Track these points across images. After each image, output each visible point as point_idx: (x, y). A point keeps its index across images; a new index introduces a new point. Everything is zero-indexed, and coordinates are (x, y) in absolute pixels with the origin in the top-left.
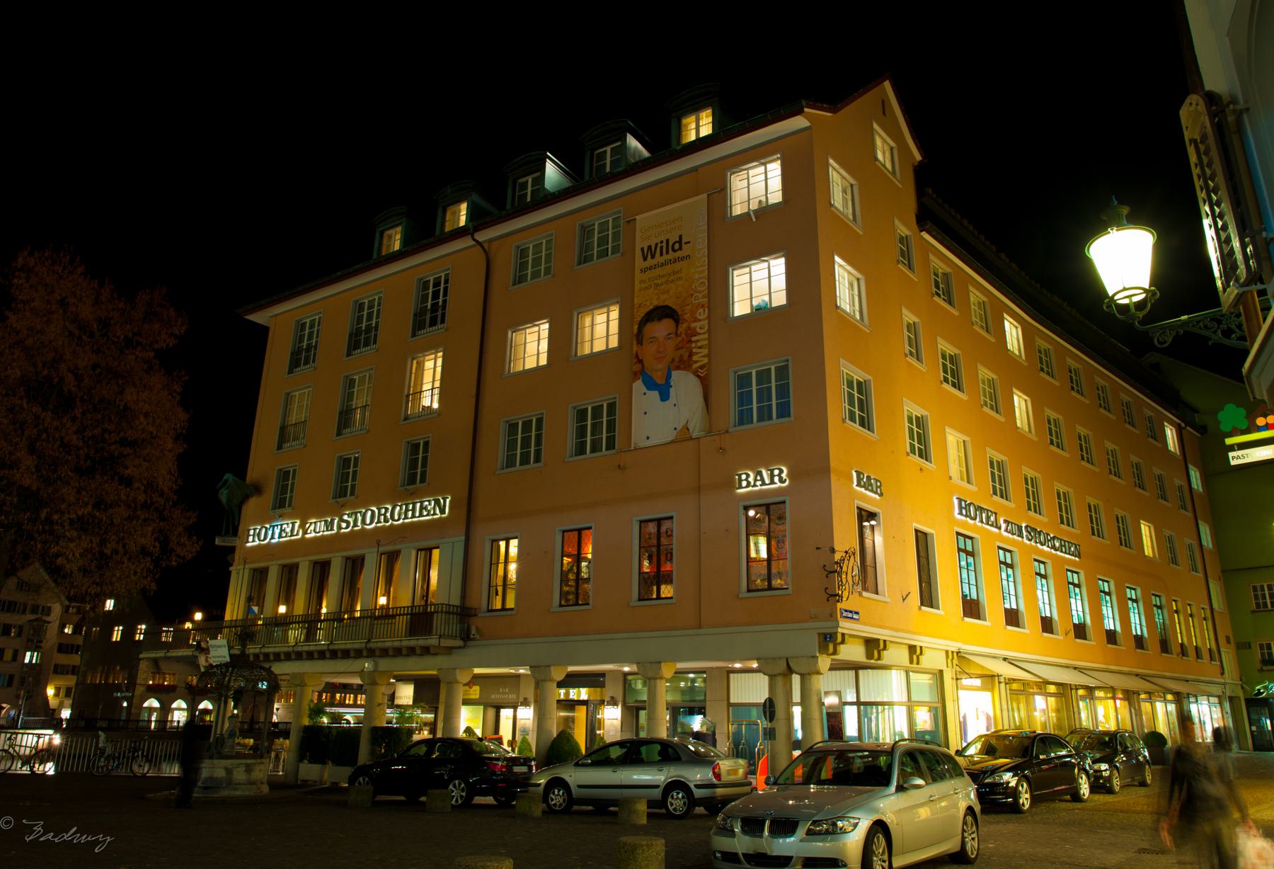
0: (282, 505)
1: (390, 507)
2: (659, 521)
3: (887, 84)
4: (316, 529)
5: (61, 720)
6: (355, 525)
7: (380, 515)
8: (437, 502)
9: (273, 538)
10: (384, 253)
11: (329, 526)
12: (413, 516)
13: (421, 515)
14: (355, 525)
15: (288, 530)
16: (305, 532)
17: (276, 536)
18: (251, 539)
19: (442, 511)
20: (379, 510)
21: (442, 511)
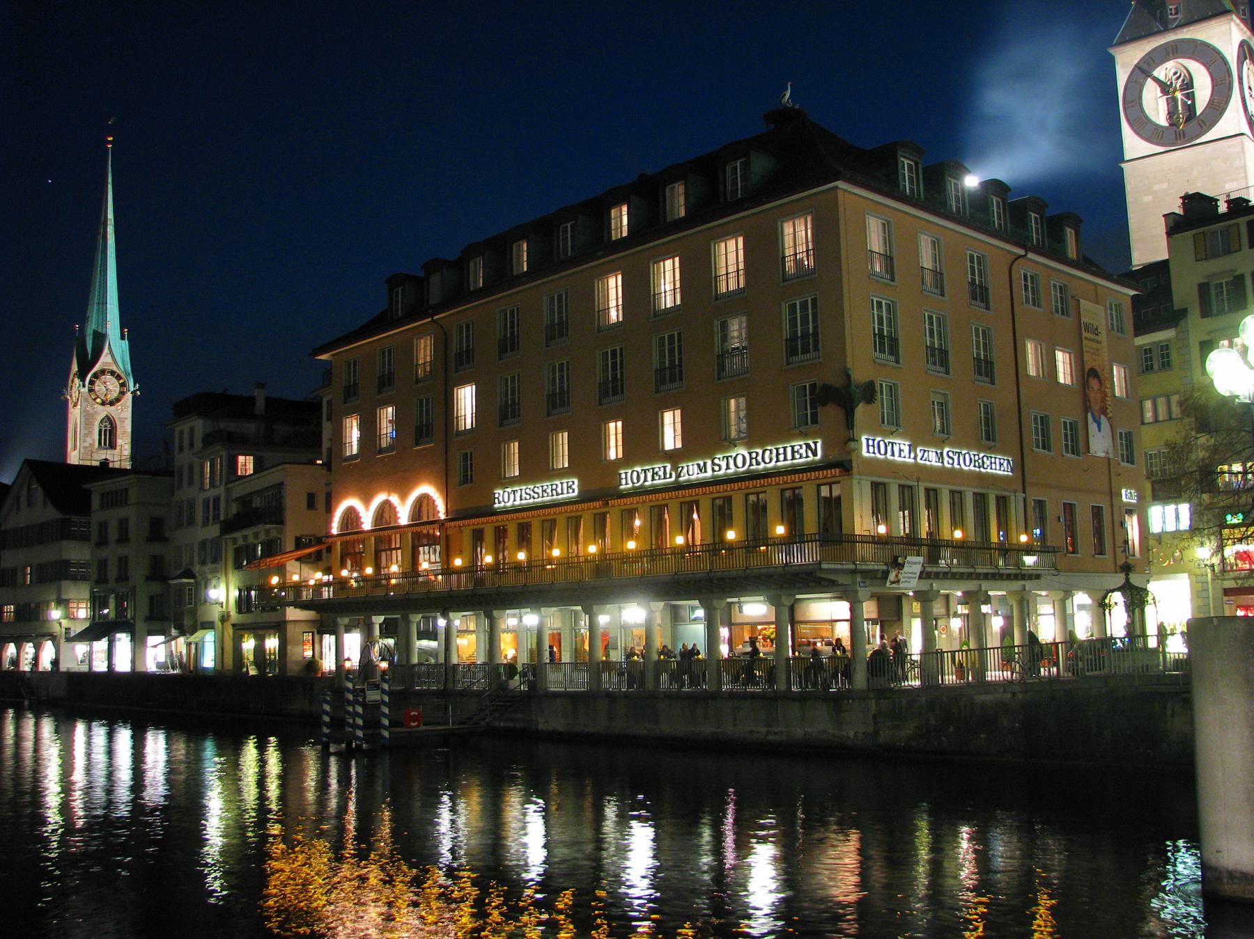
0: (891, 425)
1: (760, 451)
2: (793, 489)
3: (625, 209)
4: (930, 458)
5: (272, 588)
6: (728, 468)
7: (751, 458)
8: (808, 446)
9: (645, 480)
10: (668, 220)
11: (702, 469)
12: (785, 459)
13: (793, 458)
14: (728, 468)
15: (661, 473)
16: (679, 476)
17: (649, 478)
18: (623, 482)
19: (815, 454)
20: (750, 454)
21: (815, 454)
